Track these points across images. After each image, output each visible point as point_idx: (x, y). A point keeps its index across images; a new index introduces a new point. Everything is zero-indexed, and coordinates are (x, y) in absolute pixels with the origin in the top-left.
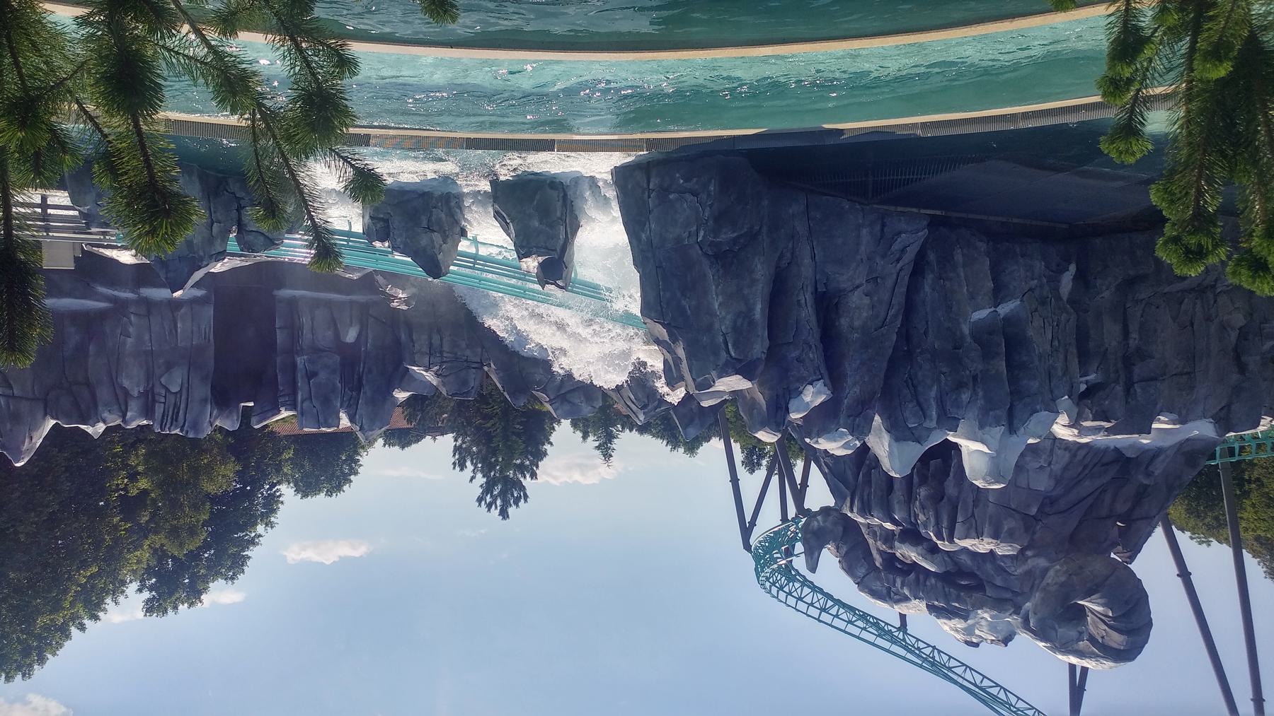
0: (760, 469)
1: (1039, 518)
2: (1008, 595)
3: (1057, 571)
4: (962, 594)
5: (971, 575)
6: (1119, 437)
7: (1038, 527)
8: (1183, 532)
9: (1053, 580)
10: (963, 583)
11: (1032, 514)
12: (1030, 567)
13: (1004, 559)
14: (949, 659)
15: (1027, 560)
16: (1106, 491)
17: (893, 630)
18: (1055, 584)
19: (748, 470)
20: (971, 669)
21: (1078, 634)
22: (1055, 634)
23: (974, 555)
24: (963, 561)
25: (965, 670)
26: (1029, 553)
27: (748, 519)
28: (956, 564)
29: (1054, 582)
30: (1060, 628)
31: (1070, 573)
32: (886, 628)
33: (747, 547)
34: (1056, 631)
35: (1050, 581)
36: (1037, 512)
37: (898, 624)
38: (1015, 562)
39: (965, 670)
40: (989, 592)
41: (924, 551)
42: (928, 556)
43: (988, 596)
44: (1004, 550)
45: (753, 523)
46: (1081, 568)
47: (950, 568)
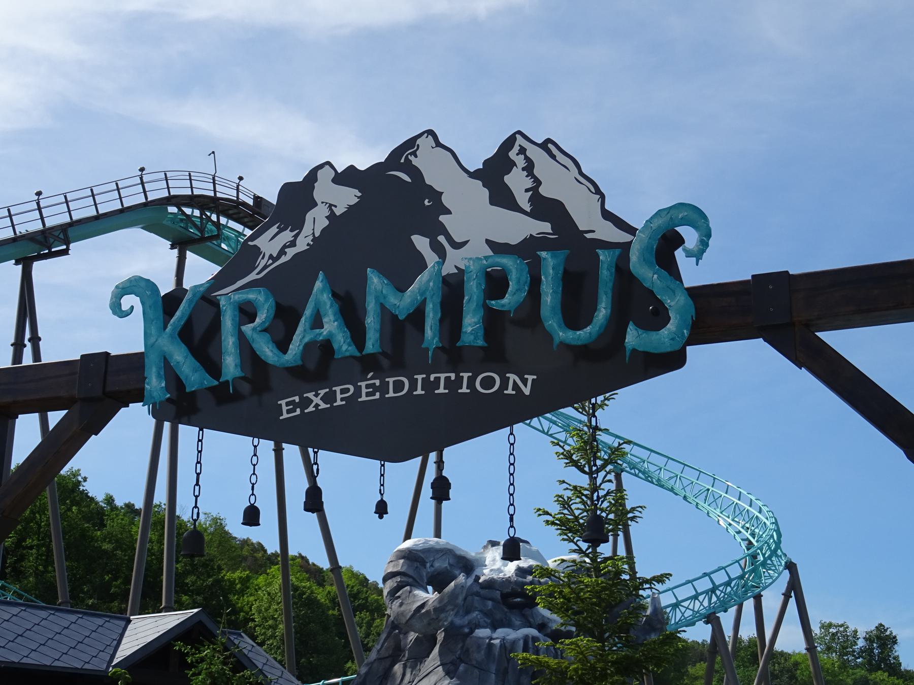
0: (867, 633)
1: (458, 661)
2: (483, 592)
3: (445, 621)
4: (519, 590)
5: (512, 607)
6: (350, 639)
7: (459, 652)
8: (300, 554)
9: (450, 613)
10: (519, 599)
11: (463, 664)
12: (466, 617)
13: (485, 625)
14: (566, 441)
15: (468, 623)
16: (409, 682)
17: (628, 469)
18: (448, 611)
19: (886, 630)
20: (543, 432)
21: (434, 565)
22: (450, 561)
23: (509, 625)
24: (518, 619)
25: (548, 431)
26: (466, 630)
27: (792, 602)
28: (524, 616)
29: (448, 613)
30: (447, 567)
31: (437, 620)
32: (637, 471)
33: (791, 567)
34: (449, 563)
35: (452, 613)
36: (459, 666)
37: (624, 475)
38: (477, 623)
39: (548, 431)
40: (497, 595)
41: (550, 625)
42: (546, 620)
43: (499, 591)
44: (483, 633)
45: (787, 596)
46: (429, 624)
47: (527, 611)
